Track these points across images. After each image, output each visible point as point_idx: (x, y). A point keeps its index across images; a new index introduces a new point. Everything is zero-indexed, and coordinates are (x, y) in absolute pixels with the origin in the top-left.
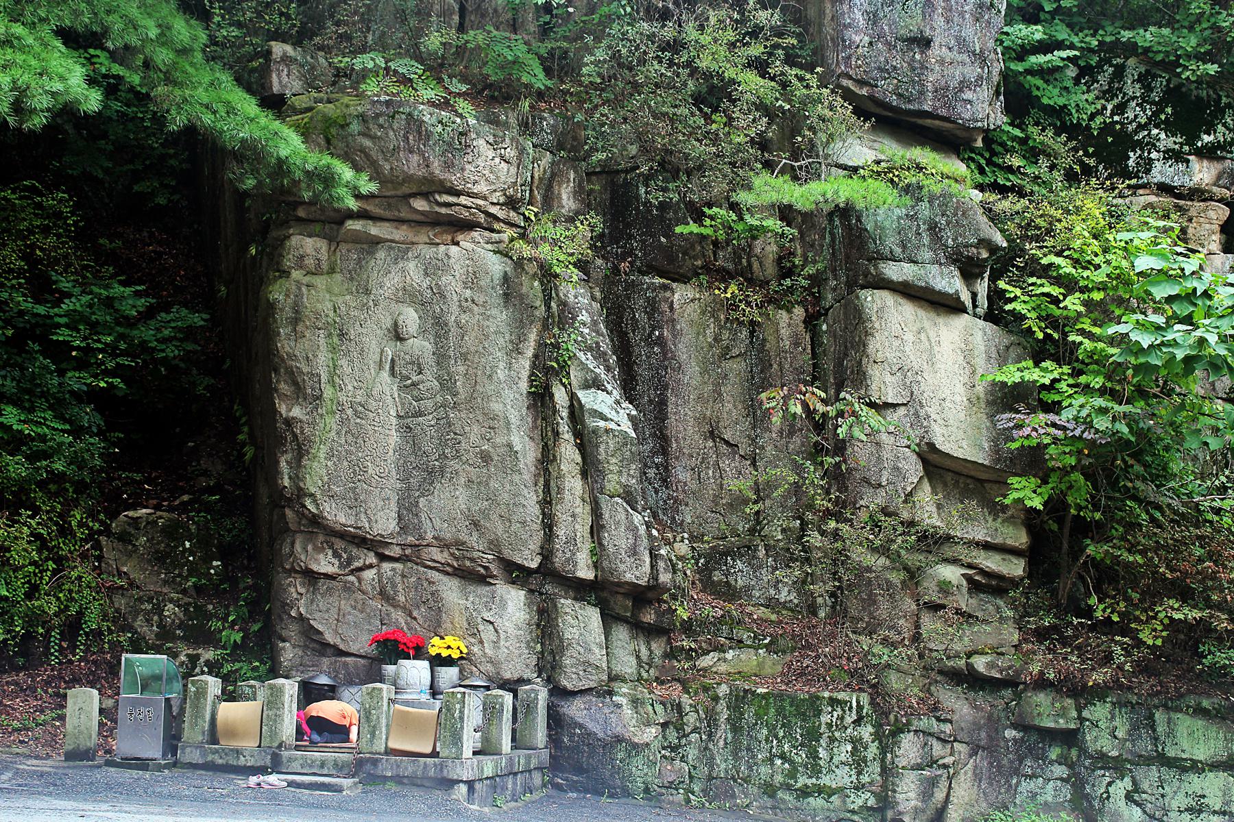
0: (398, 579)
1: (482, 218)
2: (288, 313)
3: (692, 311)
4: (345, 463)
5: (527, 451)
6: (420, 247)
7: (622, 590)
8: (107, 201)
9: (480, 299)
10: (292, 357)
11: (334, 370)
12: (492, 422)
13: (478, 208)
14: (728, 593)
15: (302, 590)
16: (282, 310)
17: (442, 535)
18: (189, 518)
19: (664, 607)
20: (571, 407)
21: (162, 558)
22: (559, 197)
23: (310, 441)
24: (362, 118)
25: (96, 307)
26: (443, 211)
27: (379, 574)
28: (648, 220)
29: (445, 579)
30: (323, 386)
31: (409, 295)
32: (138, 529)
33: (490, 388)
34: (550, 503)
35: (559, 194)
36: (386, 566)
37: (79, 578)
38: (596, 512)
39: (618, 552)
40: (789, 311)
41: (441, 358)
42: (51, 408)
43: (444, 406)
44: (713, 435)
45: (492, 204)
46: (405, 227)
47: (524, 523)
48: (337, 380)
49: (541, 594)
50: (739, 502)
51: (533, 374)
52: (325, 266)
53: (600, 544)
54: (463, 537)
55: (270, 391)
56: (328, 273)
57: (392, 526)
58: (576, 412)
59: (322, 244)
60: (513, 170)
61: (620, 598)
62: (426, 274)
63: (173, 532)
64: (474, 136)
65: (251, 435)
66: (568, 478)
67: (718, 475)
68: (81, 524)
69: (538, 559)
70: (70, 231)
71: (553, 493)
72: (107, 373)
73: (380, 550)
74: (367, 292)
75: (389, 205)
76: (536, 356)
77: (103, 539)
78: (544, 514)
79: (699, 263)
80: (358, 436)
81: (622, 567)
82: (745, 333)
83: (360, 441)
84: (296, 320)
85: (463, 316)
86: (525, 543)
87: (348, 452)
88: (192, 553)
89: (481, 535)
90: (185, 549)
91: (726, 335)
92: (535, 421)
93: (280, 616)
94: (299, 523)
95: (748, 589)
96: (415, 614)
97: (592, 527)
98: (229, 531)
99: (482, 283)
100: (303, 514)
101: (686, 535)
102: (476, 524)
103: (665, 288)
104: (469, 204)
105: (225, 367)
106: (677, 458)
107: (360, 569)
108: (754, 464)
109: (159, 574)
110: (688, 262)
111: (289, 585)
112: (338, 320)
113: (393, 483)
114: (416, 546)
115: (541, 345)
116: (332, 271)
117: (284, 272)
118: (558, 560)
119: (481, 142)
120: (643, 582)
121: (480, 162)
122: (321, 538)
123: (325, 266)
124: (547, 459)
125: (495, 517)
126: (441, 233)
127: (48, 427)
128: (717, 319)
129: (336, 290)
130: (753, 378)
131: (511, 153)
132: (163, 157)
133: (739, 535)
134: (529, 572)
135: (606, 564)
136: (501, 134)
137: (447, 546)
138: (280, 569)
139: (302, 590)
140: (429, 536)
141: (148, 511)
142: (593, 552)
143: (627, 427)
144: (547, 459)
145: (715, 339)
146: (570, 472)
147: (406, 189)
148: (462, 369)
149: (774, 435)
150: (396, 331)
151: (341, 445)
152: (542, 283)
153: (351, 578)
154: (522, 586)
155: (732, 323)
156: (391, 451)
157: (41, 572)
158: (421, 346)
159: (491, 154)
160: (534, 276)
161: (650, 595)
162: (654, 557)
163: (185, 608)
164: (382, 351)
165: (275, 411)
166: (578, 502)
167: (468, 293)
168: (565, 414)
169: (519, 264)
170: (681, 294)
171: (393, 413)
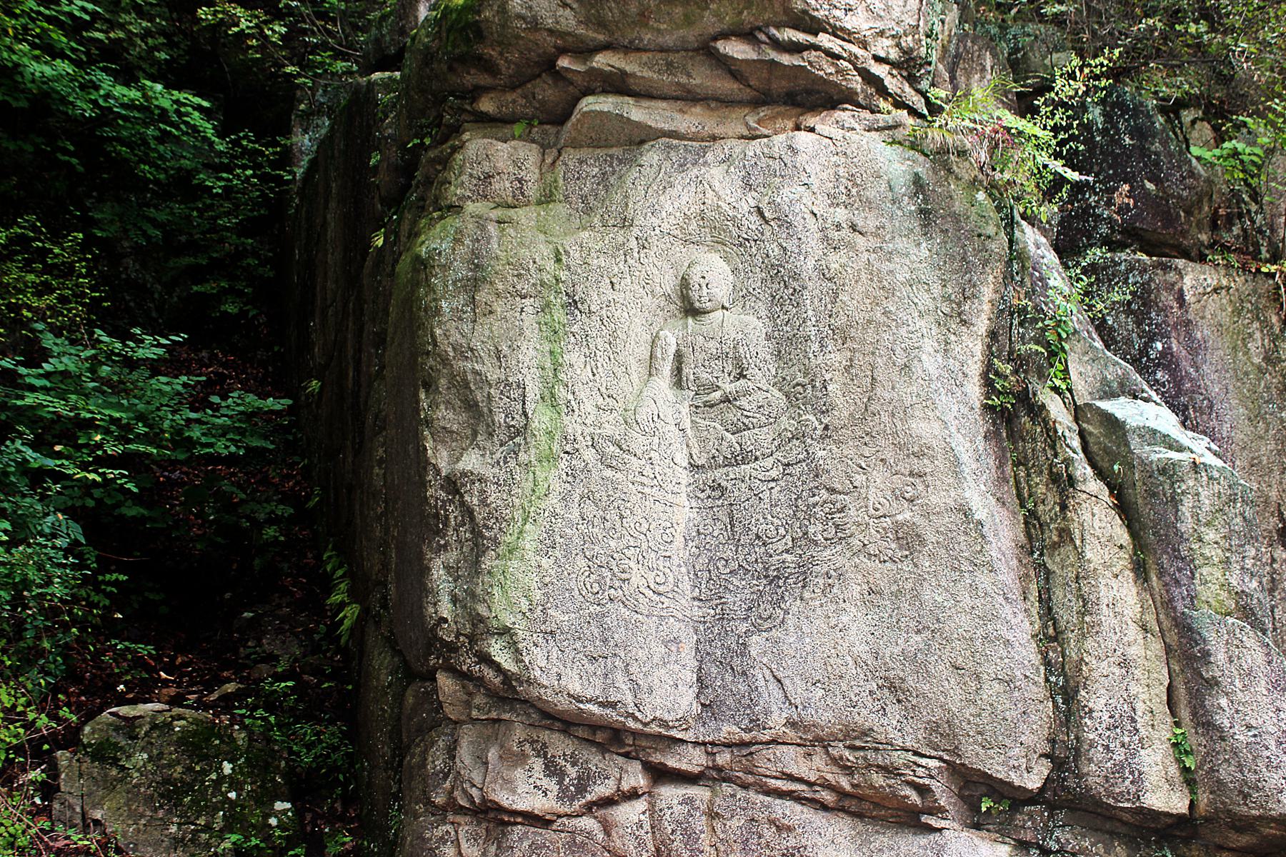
0: (700, 823)
1: (856, 83)
4: (581, 563)
6: (730, 143)
8: (154, 314)
9: (868, 221)
10: (465, 352)
13: (853, 59)
17: (809, 716)
25: (113, 389)
26: (786, 59)
28: (1116, 157)
30: (530, 407)
31: (716, 230)
32: (134, 737)
33: (907, 392)
36: (670, 794)
41: (786, 344)
43: (799, 436)
45: (877, 59)
46: (698, 110)
48: (561, 392)
51: (989, 367)
52: (532, 190)
54: (865, 717)
55: (411, 428)
56: (539, 203)
57: (686, 701)
58: (1108, 445)
59: (529, 154)
62: (748, 186)
63: (199, 746)
66: (1105, 579)
72: (111, 462)
73: (657, 758)
74: (626, 223)
75: (669, 65)
76: (993, 335)
77: (63, 756)
78: (1047, 663)
83: (612, 515)
84: (473, 285)
85: (833, 257)
87: (589, 539)
88: (235, 784)
89: (910, 712)
90: (221, 779)
92: (1001, 466)
97: (1170, 689)
98: (309, 746)
99: (871, 194)
104: (837, 50)
107: (608, 802)
109: (165, 824)
111: (442, 840)
112: (563, 275)
113: (685, 605)
114: (743, 744)
116: (547, 199)
117: (450, 207)
118: (1095, 772)
123: (532, 190)
125: (942, 670)
126: (773, 118)
128: (1265, 324)
132: (240, 254)
134: (1016, 798)
135: (1226, 773)
137: (823, 742)
138: (420, 808)
145: (1267, 359)
148: (837, 358)
151: (571, 524)
153: (587, 823)
156: (679, 542)
158: (746, 327)
165: (422, 463)
166: (1133, 632)
167: (841, 214)
170: (1194, 279)
171: (682, 459)
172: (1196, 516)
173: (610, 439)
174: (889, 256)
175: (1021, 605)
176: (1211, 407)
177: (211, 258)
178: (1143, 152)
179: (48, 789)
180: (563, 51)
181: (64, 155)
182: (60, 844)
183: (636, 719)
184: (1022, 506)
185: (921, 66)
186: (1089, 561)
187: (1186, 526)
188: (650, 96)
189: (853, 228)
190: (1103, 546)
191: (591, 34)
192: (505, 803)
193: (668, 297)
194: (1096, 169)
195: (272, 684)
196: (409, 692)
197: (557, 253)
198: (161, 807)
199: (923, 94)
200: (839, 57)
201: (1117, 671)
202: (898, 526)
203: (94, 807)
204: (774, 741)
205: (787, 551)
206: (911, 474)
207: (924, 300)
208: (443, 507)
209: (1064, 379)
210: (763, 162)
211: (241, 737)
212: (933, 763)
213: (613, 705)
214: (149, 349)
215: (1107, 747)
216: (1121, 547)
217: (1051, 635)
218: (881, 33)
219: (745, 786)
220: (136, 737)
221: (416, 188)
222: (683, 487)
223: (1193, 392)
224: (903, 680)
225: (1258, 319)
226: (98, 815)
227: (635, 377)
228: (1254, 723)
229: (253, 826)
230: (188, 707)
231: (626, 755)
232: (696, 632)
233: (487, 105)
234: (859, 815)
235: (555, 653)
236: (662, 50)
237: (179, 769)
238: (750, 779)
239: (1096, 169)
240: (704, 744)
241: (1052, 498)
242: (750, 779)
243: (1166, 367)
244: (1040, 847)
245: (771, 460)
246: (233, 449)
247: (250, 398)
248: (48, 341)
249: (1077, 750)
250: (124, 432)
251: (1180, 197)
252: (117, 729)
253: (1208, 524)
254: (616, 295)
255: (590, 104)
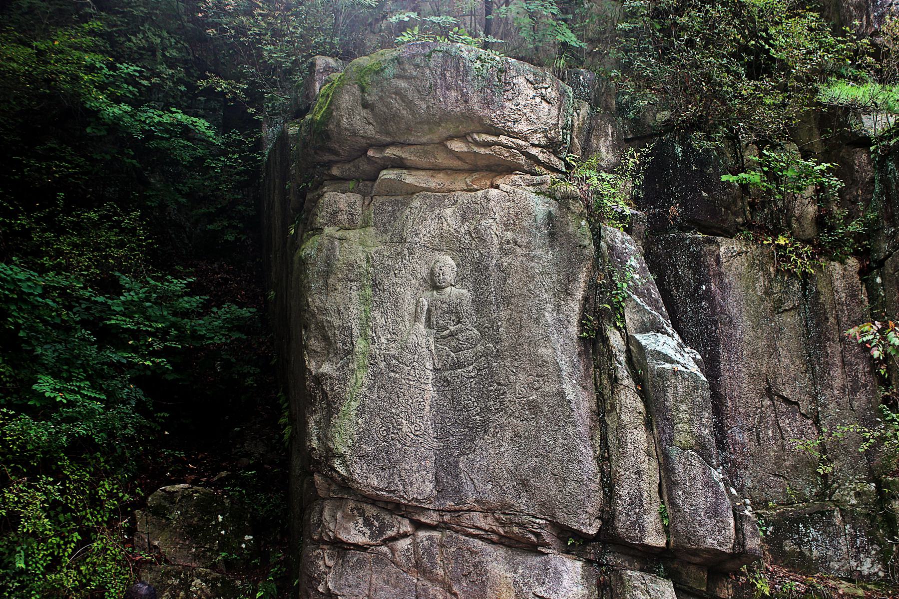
0: (436, 550)
1: (522, 160)
2: (320, 266)
3: (739, 264)
5: (582, 403)
7: (698, 560)
8: (186, 241)
10: (324, 311)
11: (366, 322)
12: (542, 369)
13: (519, 148)
14: (802, 564)
15: (330, 563)
16: (314, 264)
18: (224, 493)
19: (743, 579)
20: (628, 351)
21: (194, 533)
22: (598, 149)
23: (340, 398)
24: (398, 61)
25: (153, 303)
26: (482, 151)
27: (415, 544)
29: (489, 548)
34: (608, 459)
35: (598, 147)
36: (422, 534)
37: (104, 549)
38: (666, 467)
39: (695, 512)
40: (842, 262)
41: (480, 304)
42: (89, 378)
43: (485, 355)
44: (770, 392)
45: (533, 145)
46: (441, 175)
47: (580, 482)
48: (370, 333)
49: (601, 565)
50: (805, 464)
52: (359, 221)
53: (673, 504)
54: (510, 499)
56: (362, 227)
58: (637, 357)
59: (356, 198)
60: (554, 112)
61: (693, 569)
62: (464, 219)
63: (206, 507)
64: (513, 73)
65: (290, 417)
67: (778, 435)
68: (110, 495)
69: (597, 524)
70: (142, 246)
71: (613, 448)
72: (155, 354)
73: (416, 517)
74: (402, 240)
75: (425, 152)
76: (586, 299)
77: (138, 513)
78: (602, 471)
79: (740, 220)
80: (393, 389)
81: (702, 531)
82: (797, 286)
84: (327, 274)
85: (504, 259)
86: (582, 506)
88: (223, 526)
90: (218, 523)
91: (777, 288)
92: (587, 369)
93: (306, 592)
94: (329, 490)
95: (824, 560)
96: (455, 589)
97: (660, 485)
98: (264, 505)
99: (525, 224)
100: (332, 478)
101: (748, 501)
102: (524, 484)
103: (710, 242)
105: (273, 363)
106: (733, 418)
108: (816, 422)
109: (190, 548)
110: (731, 217)
111: (317, 557)
112: (371, 270)
114: (456, 511)
115: (592, 286)
116: (365, 225)
117: (317, 229)
118: (622, 524)
119: (521, 80)
120: (727, 549)
121: (521, 100)
122: (351, 504)
123: (359, 221)
124: (604, 408)
126: (479, 179)
127: (81, 394)
128: (766, 273)
129: (370, 243)
130: (809, 332)
131: (551, 93)
132: (234, 202)
133: (807, 501)
134: (584, 539)
135: (681, 527)
136: (542, 73)
139: (330, 563)
140: (471, 498)
141: (186, 486)
142: (662, 514)
143: (694, 368)
144: (604, 408)
145: (766, 293)
146: (632, 423)
147: (443, 131)
148: (504, 314)
149: (836, 392)
150: (432, 280)
151: (372, 401)
152: (589, 222)
153: (384, 549)
154: (579, 557)
155: (783, 276)
156: (427, 409)
157: (65, 544)
159: (531, 93)
160: (581, 214)
161: (730, 565)
162: (739, 518)
163: (212, 583)
164: (418, 302)
165: (305, 369)
166: (643, 456)
167: (509, 235)
168: (622, 358)
169: (564, 200)
170: (726, 247)
171: (429, 365)
172: (675, 397)
173: (394, 357)
174: (532, 259)
175: (589, 442)
176: (731, 322)
177: (217, 208)
178: (702, 173)
179: (132, 530)
180: (371, 146)
181: (128, 158)
182: (138, 558)
183: (404, 499)
184: (596, 390)
185: (560, 145)
186: (623, 420)
187: (670, 402)
188: (417, 169)
189: (515, 243)
190: (631, 412)
191: (383, 138)
192: (345, 539)
193: (425, 281)
194: (677, 184)
195: (244, 473)
196: (305, 482)
197: (368, 258)
198: (187, 539)
199: (564, 160)
200: (511, 148)
201: (634, 476)
202: (530, 403)
203: (154, 539)
204: (469, 510)
205: (477, 414)
206: (537, 376)
207: (548, 282)
208: (313, 391)
209: (622, 322)
210: (473, 206)
211: (227, 502)
212: (541, 522)
213: (393, 492)
214: (178, 285)
215: (627, 514)
216: (640, 413)
217: (604, 459)
218: (536, 131)
219: (457, 532)
220: (174, 503)
221: (303, 214)
222: (430, 381)
223: (722, 313)
224: (528, 481)
225: (762, 269)
226: (156, 543)
227: (407, 323)
228: (694, 503)
229: (234, 548)
230: (200, 486)
231: (402, 516)
232: (435, 454)
233: (335, 171)
234: (509, 546)
235: (365, 466)
236: (421, 145)
237: (196, 519)
238: (459, 528)
239: (677, 184)
240: (438, 510)
241: (609, 387)
242: (459, 528)
243: (707, 300)
244: (597, 563)
245: (471, 367)
246: (223, 340)
247: (234, 307)
248: (125, 280)
249: (614, 515)
250: (163, 335)
251: (722, 199)
252: (165, 498)
253: (681, 402)
254: (397, 280)
255: (388, 175)
